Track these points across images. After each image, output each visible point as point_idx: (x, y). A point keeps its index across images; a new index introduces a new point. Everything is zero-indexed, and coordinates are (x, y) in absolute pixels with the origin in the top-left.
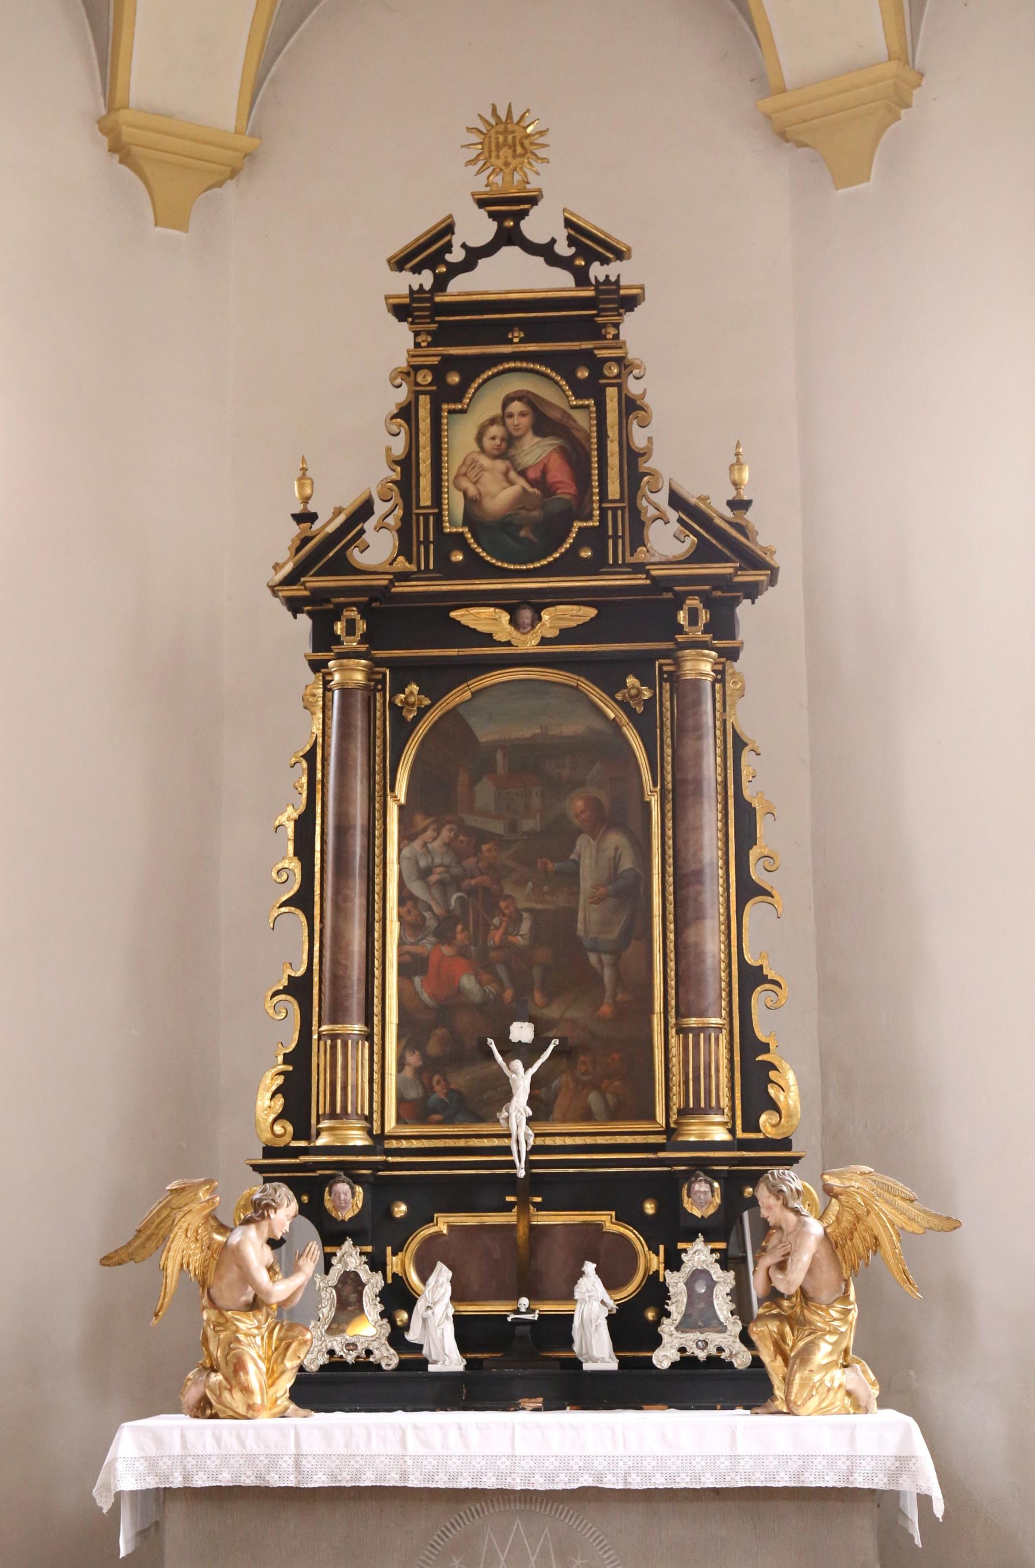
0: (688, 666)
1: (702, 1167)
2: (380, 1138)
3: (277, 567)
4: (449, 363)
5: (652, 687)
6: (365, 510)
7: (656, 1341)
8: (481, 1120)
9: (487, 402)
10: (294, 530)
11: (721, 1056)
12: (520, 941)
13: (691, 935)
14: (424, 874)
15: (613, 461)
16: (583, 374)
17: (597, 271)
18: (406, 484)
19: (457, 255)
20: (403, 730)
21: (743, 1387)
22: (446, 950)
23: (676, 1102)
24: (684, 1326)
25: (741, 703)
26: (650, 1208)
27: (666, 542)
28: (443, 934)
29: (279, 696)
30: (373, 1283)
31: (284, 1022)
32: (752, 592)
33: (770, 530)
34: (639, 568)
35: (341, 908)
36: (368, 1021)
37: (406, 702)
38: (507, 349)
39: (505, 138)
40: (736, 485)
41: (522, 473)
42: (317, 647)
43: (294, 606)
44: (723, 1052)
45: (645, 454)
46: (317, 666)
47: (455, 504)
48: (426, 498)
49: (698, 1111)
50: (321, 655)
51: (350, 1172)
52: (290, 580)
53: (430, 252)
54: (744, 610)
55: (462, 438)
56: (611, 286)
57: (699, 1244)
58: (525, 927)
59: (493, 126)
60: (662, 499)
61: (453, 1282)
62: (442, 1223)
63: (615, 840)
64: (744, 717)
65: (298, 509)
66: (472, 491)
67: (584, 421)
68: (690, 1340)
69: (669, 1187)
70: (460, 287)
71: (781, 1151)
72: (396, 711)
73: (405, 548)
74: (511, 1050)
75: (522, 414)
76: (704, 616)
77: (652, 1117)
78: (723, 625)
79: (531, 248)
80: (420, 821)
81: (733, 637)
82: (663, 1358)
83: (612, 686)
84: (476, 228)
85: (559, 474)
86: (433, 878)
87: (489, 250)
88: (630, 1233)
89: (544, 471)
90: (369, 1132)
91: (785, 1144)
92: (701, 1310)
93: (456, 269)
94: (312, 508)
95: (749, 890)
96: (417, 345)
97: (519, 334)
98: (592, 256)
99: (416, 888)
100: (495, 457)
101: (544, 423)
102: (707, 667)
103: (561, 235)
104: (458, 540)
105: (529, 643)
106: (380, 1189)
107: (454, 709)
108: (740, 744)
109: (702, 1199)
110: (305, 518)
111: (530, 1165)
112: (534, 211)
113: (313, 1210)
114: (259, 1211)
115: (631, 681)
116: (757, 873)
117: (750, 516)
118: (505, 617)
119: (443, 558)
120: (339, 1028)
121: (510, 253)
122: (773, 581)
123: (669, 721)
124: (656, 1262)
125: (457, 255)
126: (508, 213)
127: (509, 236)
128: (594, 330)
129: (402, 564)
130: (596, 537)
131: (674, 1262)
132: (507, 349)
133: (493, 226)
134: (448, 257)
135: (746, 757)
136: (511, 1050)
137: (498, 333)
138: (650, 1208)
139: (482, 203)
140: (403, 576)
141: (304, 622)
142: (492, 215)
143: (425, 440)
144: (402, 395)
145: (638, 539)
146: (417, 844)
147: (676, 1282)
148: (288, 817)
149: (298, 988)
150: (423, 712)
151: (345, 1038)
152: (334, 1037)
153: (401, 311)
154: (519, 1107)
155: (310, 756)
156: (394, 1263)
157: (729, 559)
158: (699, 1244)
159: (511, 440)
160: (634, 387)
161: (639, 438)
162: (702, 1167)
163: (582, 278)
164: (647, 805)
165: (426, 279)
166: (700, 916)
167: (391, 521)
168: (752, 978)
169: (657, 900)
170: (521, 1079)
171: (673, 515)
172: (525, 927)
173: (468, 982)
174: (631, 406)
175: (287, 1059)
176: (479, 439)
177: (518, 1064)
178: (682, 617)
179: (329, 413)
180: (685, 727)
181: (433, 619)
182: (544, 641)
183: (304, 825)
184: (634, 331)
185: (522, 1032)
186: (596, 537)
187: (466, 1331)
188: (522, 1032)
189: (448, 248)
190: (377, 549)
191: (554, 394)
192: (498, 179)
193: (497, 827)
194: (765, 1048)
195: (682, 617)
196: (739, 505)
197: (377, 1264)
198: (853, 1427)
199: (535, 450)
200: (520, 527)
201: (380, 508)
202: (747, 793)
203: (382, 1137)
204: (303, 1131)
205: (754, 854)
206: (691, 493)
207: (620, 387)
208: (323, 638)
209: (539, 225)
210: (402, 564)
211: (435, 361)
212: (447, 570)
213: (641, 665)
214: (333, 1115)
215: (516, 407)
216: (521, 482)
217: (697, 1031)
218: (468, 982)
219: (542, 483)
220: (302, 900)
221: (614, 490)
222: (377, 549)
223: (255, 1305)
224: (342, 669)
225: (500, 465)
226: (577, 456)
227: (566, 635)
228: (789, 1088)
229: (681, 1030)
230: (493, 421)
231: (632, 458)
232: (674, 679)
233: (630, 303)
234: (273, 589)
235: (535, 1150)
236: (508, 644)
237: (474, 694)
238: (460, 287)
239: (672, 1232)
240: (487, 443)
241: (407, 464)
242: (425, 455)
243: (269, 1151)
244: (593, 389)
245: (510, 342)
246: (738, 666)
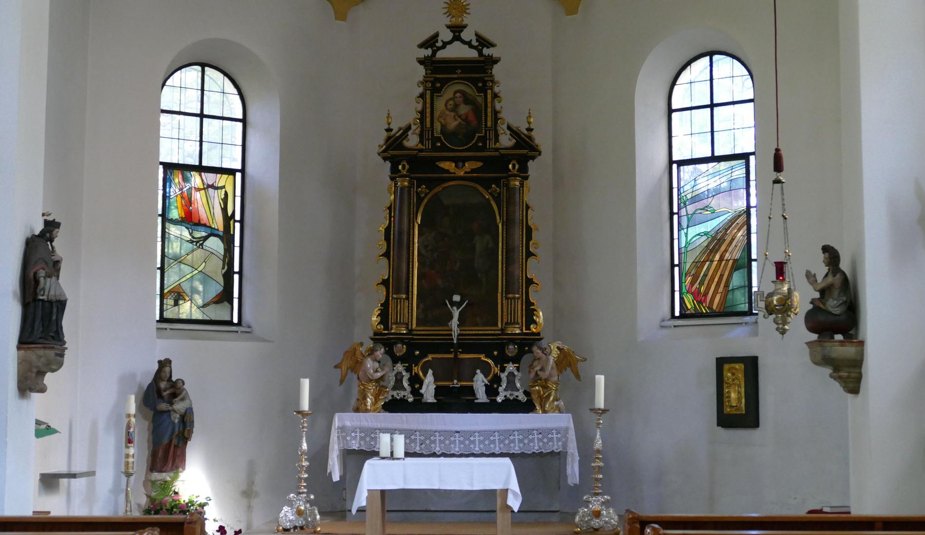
0: (512, 183)
1: (513, 341)
2: (410, 331)
3: (380, 146)
7: (498, 394)
8: (444, 326)
9: (449, 92)
11: (519, 307)
14: (426, 247)
15: (489, 114)
16: (480, 85)
17: (486, 51)
18: (422, 120)
19: (439, 44)
20: (420, 200)
21: (527, 407)
23: (505, 320)
24: (505, 390)
26: (495, 353)
27: (506, 140)
29: (379, 187)
30: (406, 376)
31: (381, 294)
32: (533, 158)
33: (541, 138)
34: (497, 150)
35: (400, 258)
36: (407, 294)
38: (455, 76)
40: (529, 123)
41: (460, 117)
42: (392, 173)
43: (385, 159)
44: (520, 306)
46: (392, 179)
48: (428, 125)
49: (511, 323)
51: (402, 341)
52: (384, 151)
53: (430, 43)
54: (530, 164)
55: (440, 104)
57: (511, 364)
58: (458, 264)
59: (673, 316)
60: (505, 127)
61: (433, 374)
62: (430, 357)
65: (387, 127)
66: (443, 122)
67: (480, 100)
68: (508, 394)
69: (502, 347)
71: (536, 338)
72: (418, 194)
73: (421, 142)
74: (453, 304)
76: (517, 166)
77: (497, 325)
78: (524, 169)
82: (499, 399)
83: (487, 188)
84: (446, 35)
85: (472, 117)
87: (450, 42)
88: (490, 361)
90: (407, 328)
91: (539, 334)
92: (515, 380)
93: (439, 48)
94: (391, 127)
95: (529, 254)
97: (460, 74)
99: (423, 252)
101: (467, 100)
102: (517, 183)
103: (474, 38)
104: (439, 139)
105: (462, 174)
106: (412, 345)
109: (512, 350)
110: (389, 130)
111: (458, 339)
112: (465, 30)
113: (390, 353)
114: (371, 352)
117: (533, 133)
118: (454, 165)
119: (434, 145)
120: (398, 296)
121: (457, 44)
122: (540, 154)
124: (497, 370)
125: (439, 44)
126: (457, 30)
127: (457, 38)
128: (484, 71)
129: (420, 146)
131: (503, 370)
132: (455, 76)
135: (530, 212)
136: (453, 304)
137: (452, 70)
138: (495, 353)
139: (448, 27)
140: (421, 151)
141: (388, 164)
143: (428, 105)
144: (421, 90)
145: (497, 140)
147: (503, 376)
148: (382, 229)
149: (385, 283)
150: (426, 194)
151: (401, 299)
152: (397, 299)
153: (421, 62)
154: (455, 322)
155: (390, 208)
156: (415, 369)
157: (526, 148)
158: (511, 364)
160: (496, 89)
161: (498, 107)
162: (513, 341)
163: (480, 53)
165: (429, 52)
168: (530, 282)
169: (500, 257)
170: (456, 313)
172: (458, 264)
173: (439, 282)
174: (495, 96)
175: (382, 305)
176: (446, 105)
177: (455, 308)
178: (510, 166)
179: (395, 96)
180: (510, 201)
182: (466, 173)
183: (388, 230)
184: (496, 70)
185: (457, 298)
186: (483, 139)
187: (438, 391)
188: (457, 298)
189: (437, 41)
190: (412, 141)
191: (470, 90)
192: (454, 19)
194: (533, 304)
195: (510, 166)
197: (409, 370)
198: (405, 483)
199: (464, 109)
201: (413, 127)
202: (530, 223)
203: (412, 330)
204: (386, 328)
206: (514, 125)
208: (394, 170)
209: (467, 35)
210: (420, 146)
212: (434, 149)
213: (497, 181)
214: (396, 323)
215: (458, 95)
216: (459, 120)
217: (511, 299)
218: (439, 282)
220: (387, 255)
221: (489, 124)
222: (412, 141)
223: (371, 381)
225: (453, 114)
227: (473, 171)
228: (540, 317)
229: (507, 298)
230: (450, 99)
231: (496, 113)
232: (507, 185)
233: (496, 61)
234: (379, 154)
235: (459, 335)
238: (441, 55)
239: (502, 360)
240: (449, 107)
241: (422, 113)
242: (428, 110)
243: (375, 334)
244: (483, 90)
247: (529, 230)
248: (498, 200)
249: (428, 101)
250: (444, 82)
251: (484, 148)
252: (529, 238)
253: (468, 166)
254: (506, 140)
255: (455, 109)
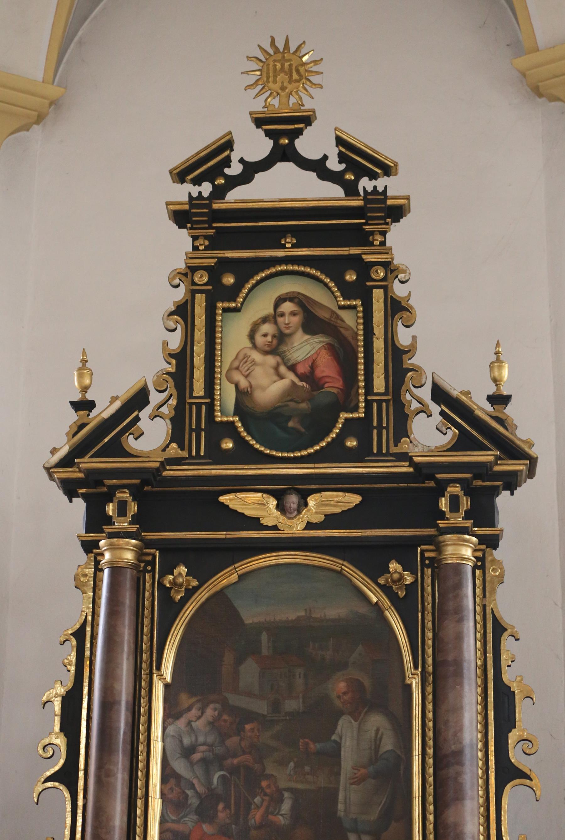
0: (449, 550)
4: (225, 265)
5: (414, 572)
6: (140, 399)
10: (72, 417)
12: (281, 820)
13: (450, 816)
14: (187, 752)
18: (180, 376)
19: (235, 169)
20: (170, 610)
22: (207, 828)
25: (500, 589)
27: (428, 435)
28: (205, 812)
32: (511, 482)
37: (174, 583)
38: (280, 253)
39: (282, 65)
40: (496, 381)
41: (292, 368)
45: (410, 351)
46: (89, 547)
47: (227, 396)
48: (199, 389)
50: (93, 536)
52: (67, 462)
53: (210, 165)
54: (503, 500)
55: (235, 335)
56: (379, 196)
60: (425, 393)
63: (376, 721)
64: (506, 603)
66: (243, 383)
67: (351, 320)
70: (237, 196)
72: (165, 591)
73: (177, 435)
75: (293, 314)
78: (483, 514)
79: (305, 164)
80: (185, 700)
81: (492, 523)
83: (375, 571)
84: (254, 145)
85: (327, 368)
86: (197, 756)
87: (265, 165)
89: (313, 367)
95: (508, 773)
96: (195, 248)
98: (362, 172)
100: (266, 353)
101: (312, 323)
102: (468, 552)
104: (229, 429)
105: (295, 528)
107: (221, 593)
108: (499, 629)
110: (83, 406)
112: (308, 131)
115: (394, 566)
116: (515, 756)
123: (431, 604)
125: (235, 169)
126: (284, 132)
127: (284, 153)
130: (360, 429)
133: (270, 144)
134: (227, 171)
135: (506, 642)
137: (273, 238)
141: (80, 505)
142: (268, 134)
144: (180, 294)
145: (402, 429)
146: (181, 723)
150: (190, 593)
155: (79, 634)
159: (282, 337)
160: (399, 290)
161: (403, 337)
163: (351, 190)
164: (408, 688)
166: (459, 797)
167: (165, 410)
171: (435, 409)
174: (397, 308)
176: (252, 336)
180: (446, 610)
181: (203, 503)
182: (310, 526)
183: (72, 702)
189: (227, 162)
190: (151, 437)
193: (261, 707)
196: (499, 400)
199: (305, 347)
200: (289, 418)
201: (155, 398)
202: (507, 677)
205: (513, 736)
206: (455, 388)
207: (386, 289)
208: (96, 520)
211: (211, 262)
212: (217, 456)
213: (404, 550)
219: (310, 377)
220: (67, 776)
221: (379, 384)
222: (151, 437)
224: (112, 548)
225: (271, 360)
226: (343, 352)
227: (331, 521)
230: (265, 320)
231: (397, 355)
236: (275, 528)
237: (242, 577)
238: (237, 196)
240: (259, 340)
241: (182, 358)
242: (199, 348)
244: (361, 291)
245: (284, 247)
246: (497, 554)
247: (503, 706)
248: (407, 606)
249: (200, 320)
250: (245, 270)
251: (362, 454)
252: (505, 719)
253: (317, 506)
254: (428, 435)
255: (278, 345)
